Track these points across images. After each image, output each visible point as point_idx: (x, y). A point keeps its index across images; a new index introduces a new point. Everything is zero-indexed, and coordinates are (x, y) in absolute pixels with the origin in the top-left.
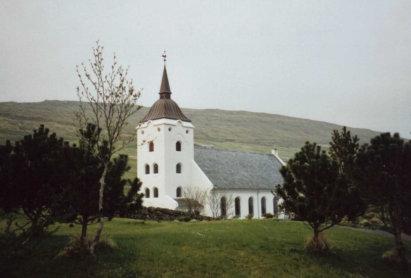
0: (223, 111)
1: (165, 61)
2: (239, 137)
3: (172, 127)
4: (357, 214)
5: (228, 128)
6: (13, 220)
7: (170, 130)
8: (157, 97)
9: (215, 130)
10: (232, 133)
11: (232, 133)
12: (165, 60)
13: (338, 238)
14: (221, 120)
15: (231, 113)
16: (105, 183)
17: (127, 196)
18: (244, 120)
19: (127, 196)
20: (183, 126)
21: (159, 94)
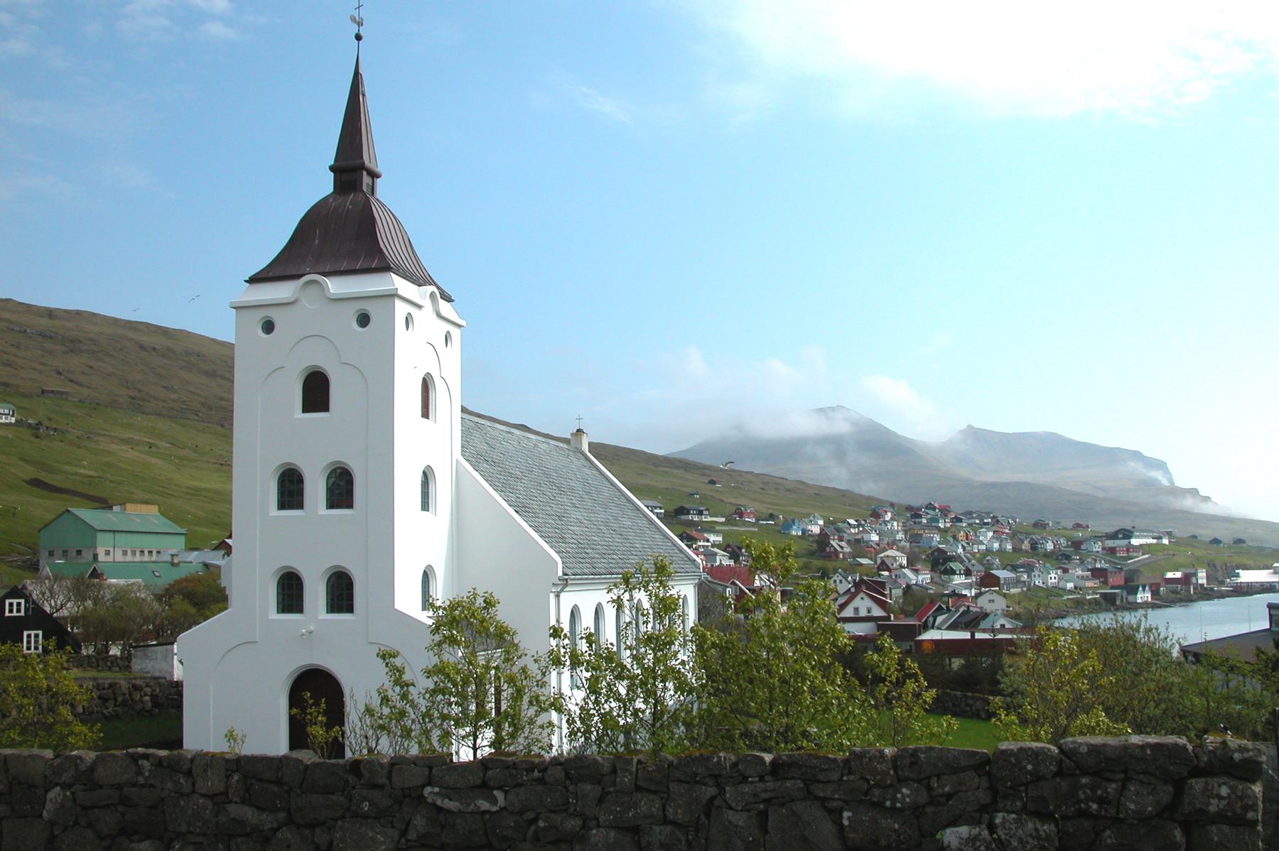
0: (29, 306)
1: (360, 42)
2: (81, 385)
3: (276, 316)
4: (118, 642)
5: (43, 356)
6: (506, 796)
7: (269, 327)
8: (324, 185)
9: (8, 360)
10: (59, 373)
11: (59, 373)
12: (358, 37)
13: (309, 772)
14: (21, 332)
15: (50, 313)
16: (1175, 653)
17: (1237, 760)
18: (90, 339)
19: (1237, 760)
20: (439, 315)
21: (332, 169)
